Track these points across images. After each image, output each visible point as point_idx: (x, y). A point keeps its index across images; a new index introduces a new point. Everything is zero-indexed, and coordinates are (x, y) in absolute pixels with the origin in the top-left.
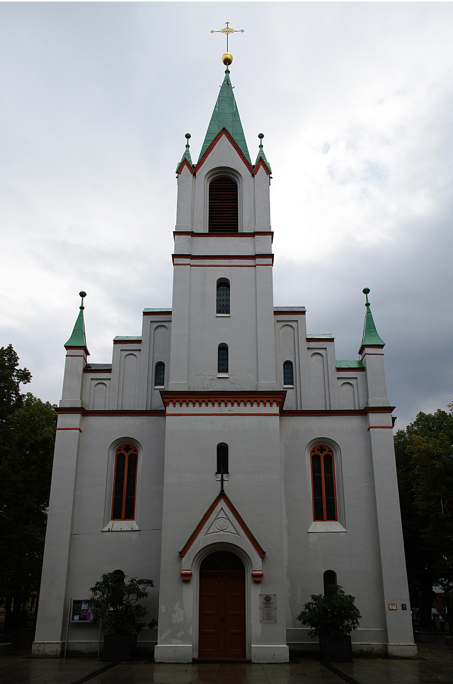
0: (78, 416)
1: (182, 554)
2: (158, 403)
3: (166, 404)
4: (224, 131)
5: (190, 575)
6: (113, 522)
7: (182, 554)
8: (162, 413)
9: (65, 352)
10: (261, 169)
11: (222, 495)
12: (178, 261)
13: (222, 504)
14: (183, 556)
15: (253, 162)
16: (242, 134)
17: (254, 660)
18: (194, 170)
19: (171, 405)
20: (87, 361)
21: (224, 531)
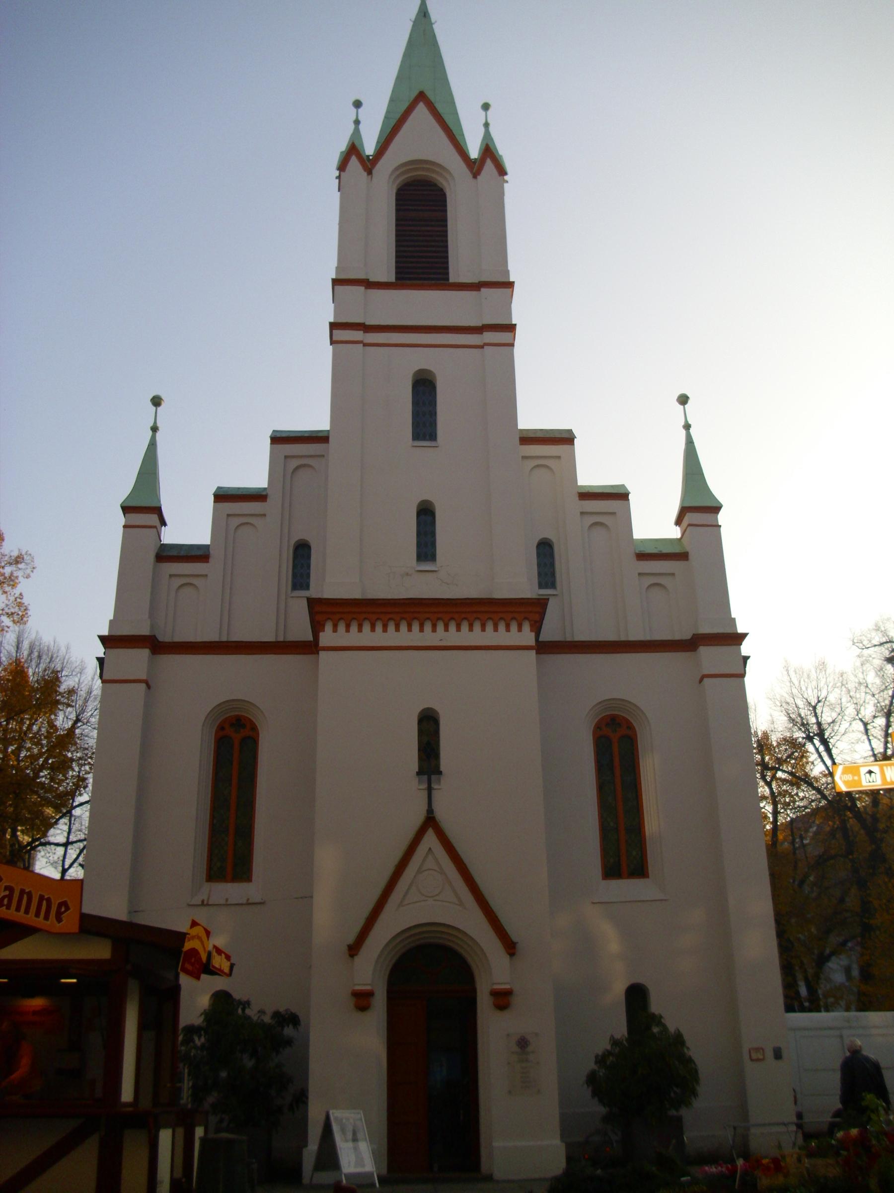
0: (145, 653)
1: (354, 949)
2: (301, 630)
3: (317, 627)
4: (421, 97)
5: (369, 994)
6: (210, 891)
7: (354, 949)
8: (311, 648)
9: (120, 519)
10: (489, 164)
11: (430, 821)
12: (340, 334)
13: (430, 839)
14: (356, 955)
15: (474, 153)
16: (455, 113)
17: (498, 1175)
18: (369, 165)
19: (329, 627)
20: (162, 539)
21: (437, 898)
